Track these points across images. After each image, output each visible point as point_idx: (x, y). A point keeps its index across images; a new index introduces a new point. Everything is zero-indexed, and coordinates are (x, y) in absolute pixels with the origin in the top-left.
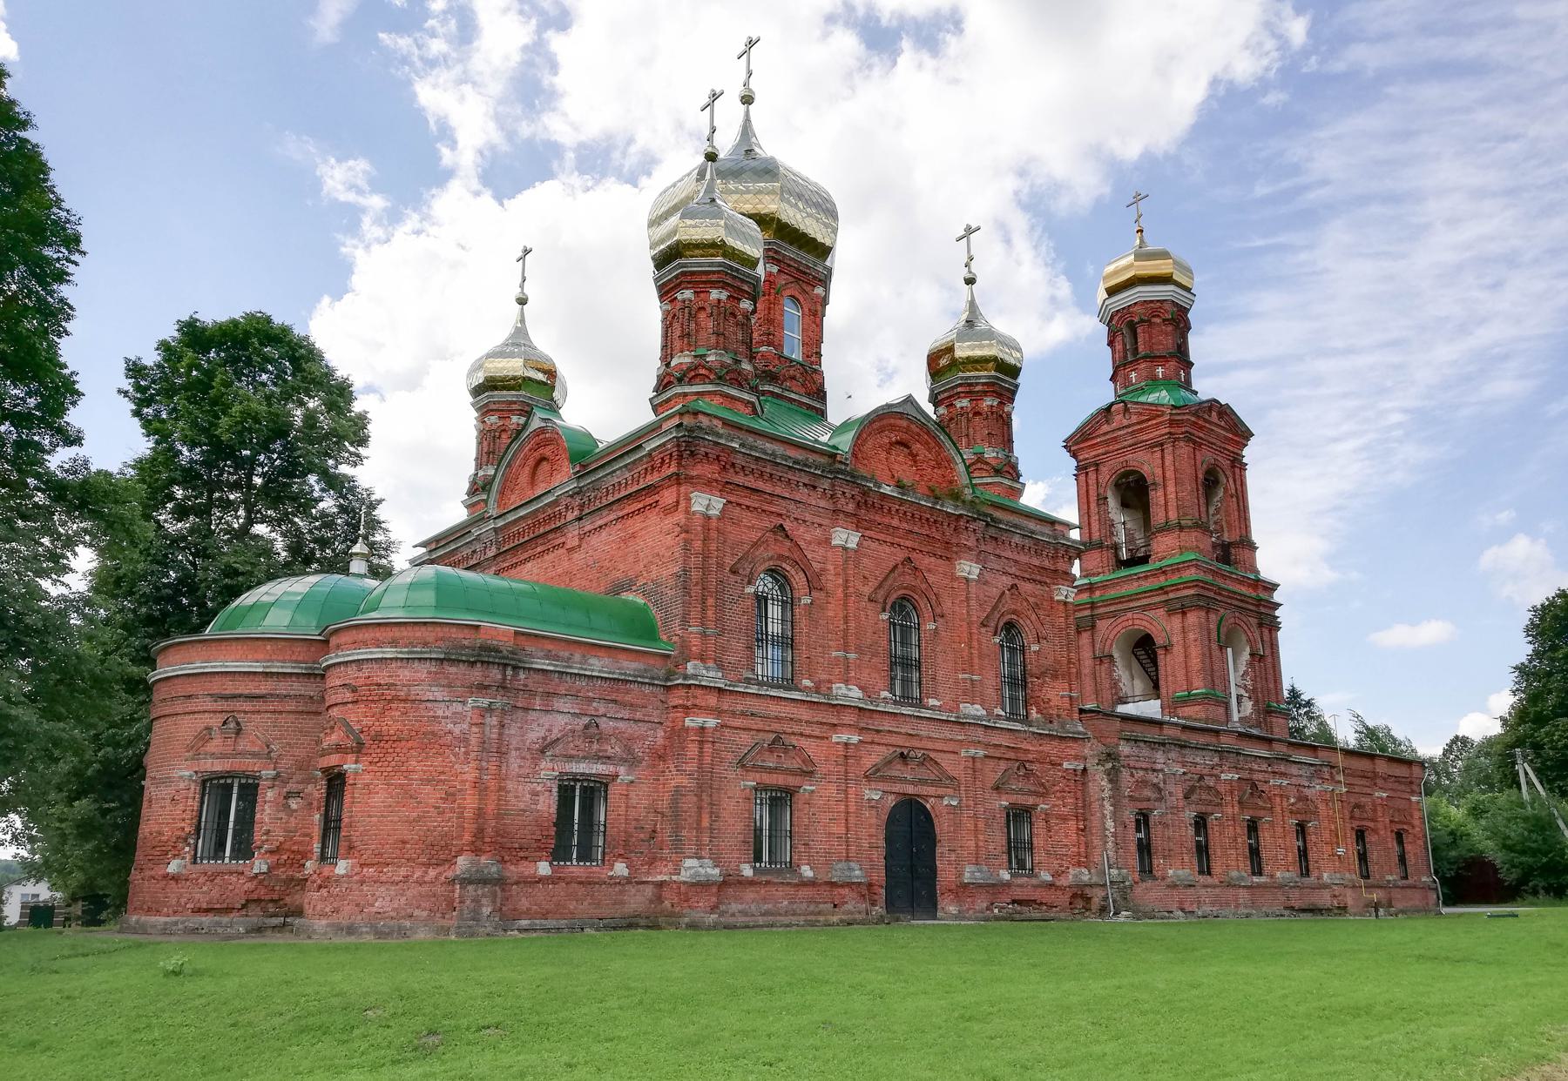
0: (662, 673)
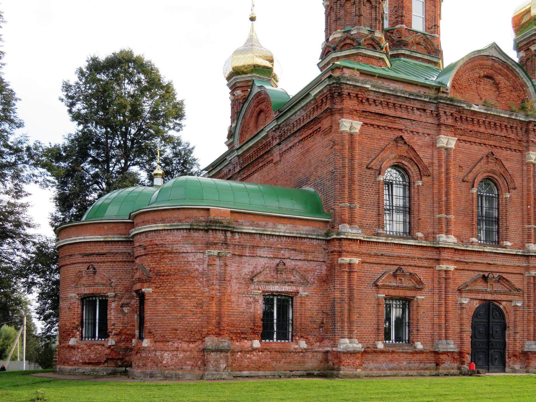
0: (323, 232)
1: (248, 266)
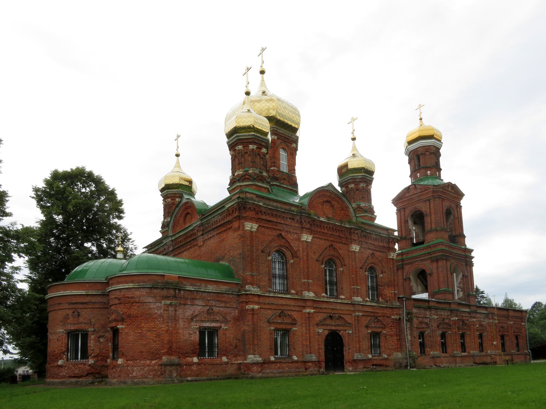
1: (189, 312)
